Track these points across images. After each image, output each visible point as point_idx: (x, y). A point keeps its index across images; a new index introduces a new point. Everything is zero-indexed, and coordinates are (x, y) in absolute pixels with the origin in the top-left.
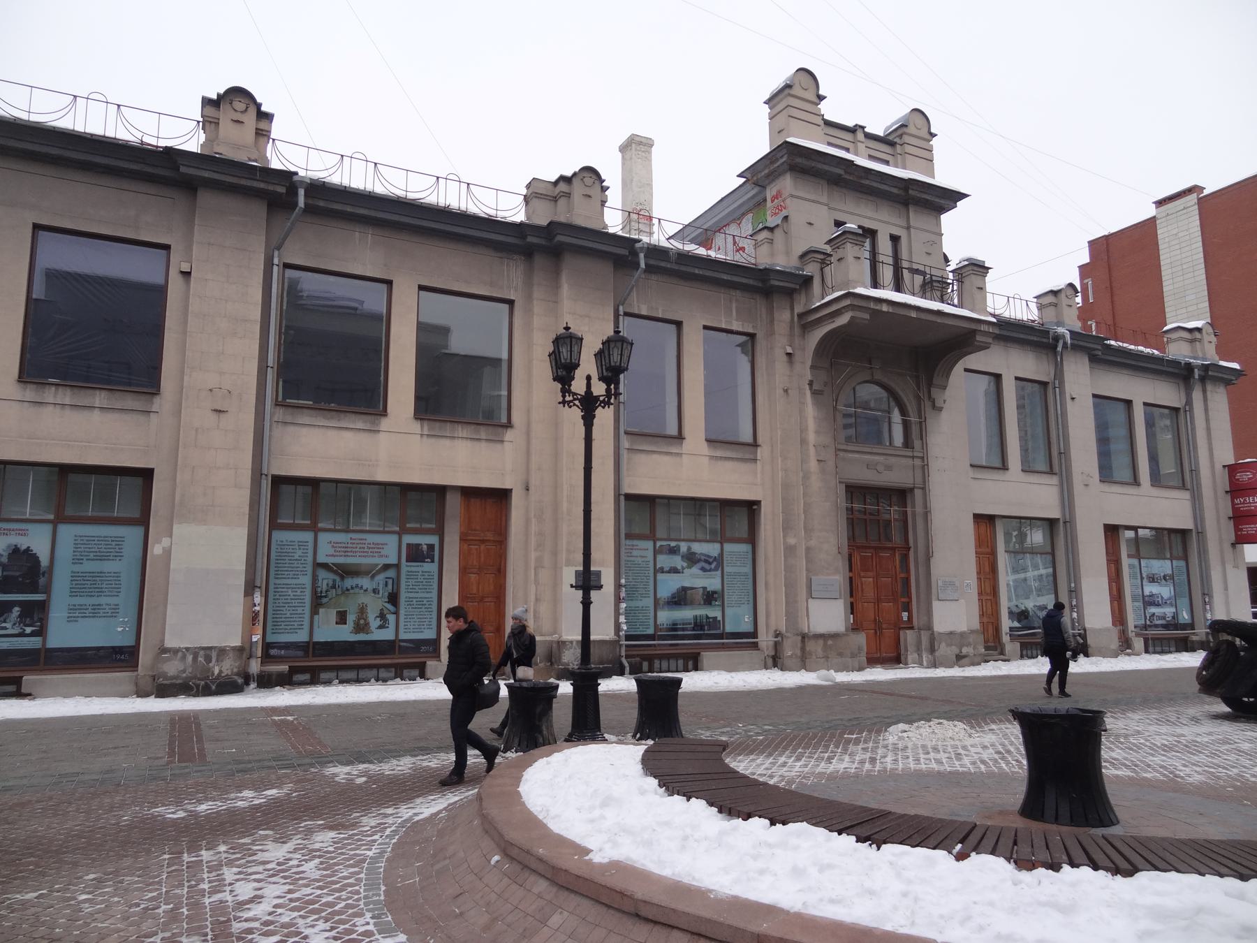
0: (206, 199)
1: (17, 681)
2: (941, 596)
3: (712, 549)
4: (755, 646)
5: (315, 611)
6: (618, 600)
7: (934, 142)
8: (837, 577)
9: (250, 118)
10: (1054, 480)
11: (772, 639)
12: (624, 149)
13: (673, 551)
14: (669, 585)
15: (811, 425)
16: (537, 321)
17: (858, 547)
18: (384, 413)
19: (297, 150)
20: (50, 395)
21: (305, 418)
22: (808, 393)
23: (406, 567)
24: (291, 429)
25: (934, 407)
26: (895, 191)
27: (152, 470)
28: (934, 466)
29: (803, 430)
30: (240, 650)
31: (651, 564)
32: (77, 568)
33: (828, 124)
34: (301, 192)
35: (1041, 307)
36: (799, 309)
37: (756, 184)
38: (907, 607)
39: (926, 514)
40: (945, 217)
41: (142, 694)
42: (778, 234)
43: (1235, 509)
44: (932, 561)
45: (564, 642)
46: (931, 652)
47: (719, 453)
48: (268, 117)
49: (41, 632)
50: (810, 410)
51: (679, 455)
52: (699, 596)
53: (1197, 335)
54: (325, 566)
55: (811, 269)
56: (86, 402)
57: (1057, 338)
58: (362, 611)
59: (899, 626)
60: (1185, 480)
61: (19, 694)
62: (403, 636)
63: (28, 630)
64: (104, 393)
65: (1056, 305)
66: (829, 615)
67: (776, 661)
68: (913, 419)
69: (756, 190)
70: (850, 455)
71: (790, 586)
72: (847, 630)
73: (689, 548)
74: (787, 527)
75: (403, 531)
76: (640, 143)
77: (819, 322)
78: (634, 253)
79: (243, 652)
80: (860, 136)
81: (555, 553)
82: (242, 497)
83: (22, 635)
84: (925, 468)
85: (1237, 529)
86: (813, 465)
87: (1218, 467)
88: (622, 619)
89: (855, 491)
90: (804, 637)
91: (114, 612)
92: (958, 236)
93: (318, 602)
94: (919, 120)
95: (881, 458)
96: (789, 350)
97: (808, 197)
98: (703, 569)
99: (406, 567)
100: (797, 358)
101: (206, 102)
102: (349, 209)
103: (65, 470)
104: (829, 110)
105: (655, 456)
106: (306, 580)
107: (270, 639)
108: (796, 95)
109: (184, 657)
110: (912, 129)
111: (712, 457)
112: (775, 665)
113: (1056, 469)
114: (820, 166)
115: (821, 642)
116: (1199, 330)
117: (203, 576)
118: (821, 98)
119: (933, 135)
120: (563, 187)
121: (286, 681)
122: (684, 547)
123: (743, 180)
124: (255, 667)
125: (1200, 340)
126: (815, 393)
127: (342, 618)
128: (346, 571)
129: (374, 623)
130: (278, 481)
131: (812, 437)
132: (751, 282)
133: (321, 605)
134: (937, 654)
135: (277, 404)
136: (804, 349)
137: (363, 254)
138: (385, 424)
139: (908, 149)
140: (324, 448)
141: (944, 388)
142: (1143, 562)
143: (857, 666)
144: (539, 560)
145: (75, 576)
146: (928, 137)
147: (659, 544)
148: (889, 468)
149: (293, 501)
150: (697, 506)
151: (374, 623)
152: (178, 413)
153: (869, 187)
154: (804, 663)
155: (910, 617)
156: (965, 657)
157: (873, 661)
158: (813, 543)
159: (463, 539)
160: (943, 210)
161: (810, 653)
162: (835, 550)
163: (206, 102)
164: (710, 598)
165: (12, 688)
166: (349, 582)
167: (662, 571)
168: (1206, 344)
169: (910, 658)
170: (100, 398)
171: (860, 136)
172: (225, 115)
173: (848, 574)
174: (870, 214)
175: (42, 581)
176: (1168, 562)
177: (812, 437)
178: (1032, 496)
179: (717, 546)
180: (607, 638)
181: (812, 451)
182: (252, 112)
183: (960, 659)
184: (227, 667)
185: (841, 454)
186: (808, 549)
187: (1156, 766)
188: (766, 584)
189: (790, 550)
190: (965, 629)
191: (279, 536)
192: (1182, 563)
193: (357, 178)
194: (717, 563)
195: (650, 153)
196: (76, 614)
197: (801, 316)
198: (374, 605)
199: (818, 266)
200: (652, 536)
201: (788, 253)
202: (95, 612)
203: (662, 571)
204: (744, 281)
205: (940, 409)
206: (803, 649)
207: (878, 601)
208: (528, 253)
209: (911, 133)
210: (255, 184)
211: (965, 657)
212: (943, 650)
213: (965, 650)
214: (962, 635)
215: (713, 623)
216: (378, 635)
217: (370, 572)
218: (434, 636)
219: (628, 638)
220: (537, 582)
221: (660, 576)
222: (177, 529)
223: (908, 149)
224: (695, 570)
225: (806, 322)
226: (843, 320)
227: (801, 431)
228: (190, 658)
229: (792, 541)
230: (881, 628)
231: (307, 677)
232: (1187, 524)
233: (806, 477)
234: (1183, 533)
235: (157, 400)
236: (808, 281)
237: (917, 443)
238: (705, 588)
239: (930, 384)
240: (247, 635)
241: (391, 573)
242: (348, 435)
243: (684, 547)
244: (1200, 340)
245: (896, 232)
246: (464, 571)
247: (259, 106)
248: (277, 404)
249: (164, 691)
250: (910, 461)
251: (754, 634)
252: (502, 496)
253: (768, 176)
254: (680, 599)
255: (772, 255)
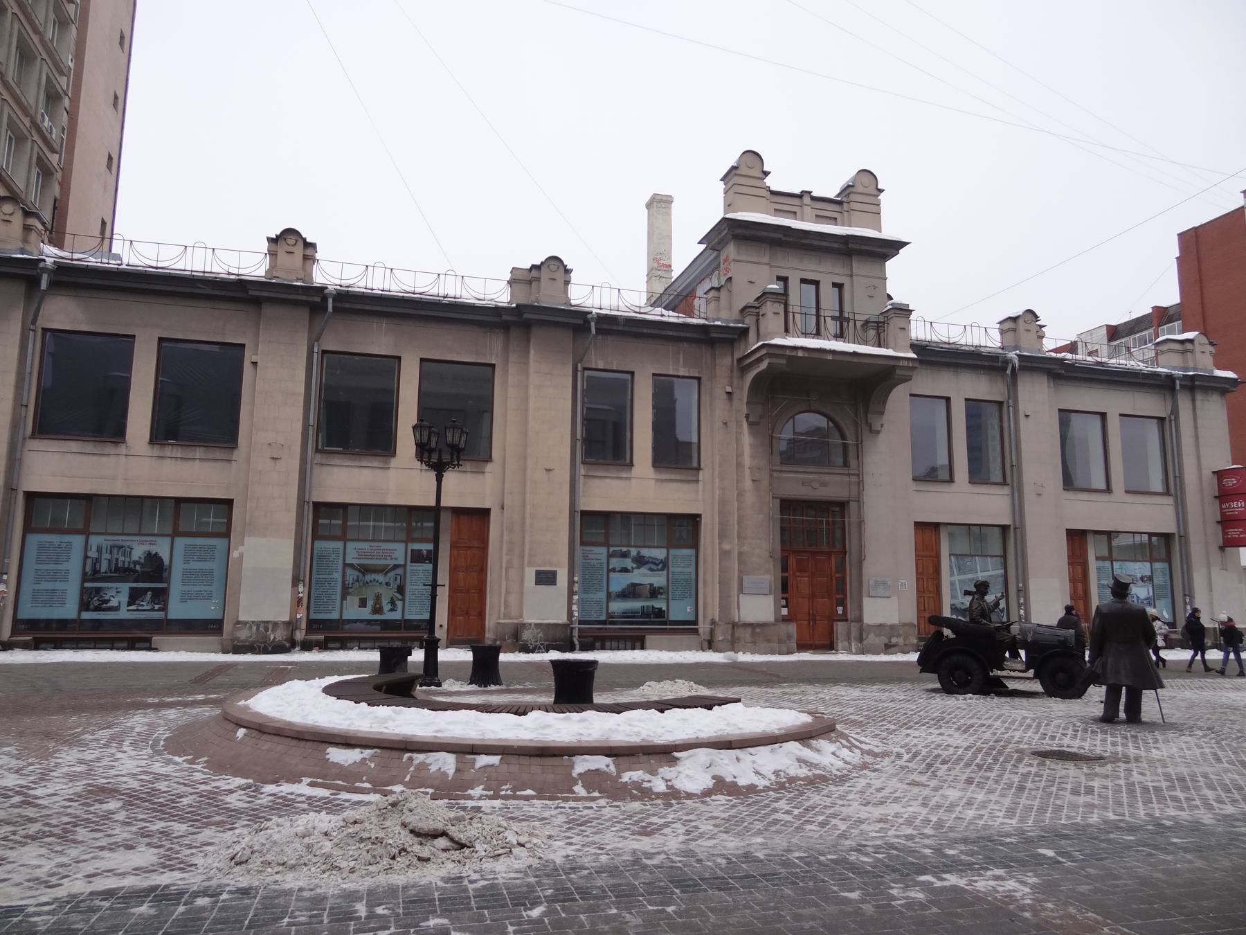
0: (268, 310)
1: (149, 640)
2: (872, 593)
3: (659, 554)
4: (696, 632)
5: (343, 598)
6: (571, 593)
7: (882, 197)
8: (768, 577)
9: (299, 251)
10: (1006, 490)
11: (708, 626)
12: (649, 205)
13: (625, 555)
14: (619, 582)
15: (747, 450)
16: (511, 380)
17: (794, 552)
18: (393, 454)
19: (329, 273)
20: (168, 451)
21: (337, 460)
22: (745, 425)
23: (410, 567)
24: (326, 469)
25: (871, 430)
26: (836, 246)
27: (232, 501)
28: (868, 481)
29: (739, 455)
30: (288, 624)
31: (605, 566)
32: (186, 566)
33: (774, 193)
34: (330, 301)
35: (1002, 332)
36: (737, 355)
37: (713, 249)
38: (842, 602)
39: (860, 523)
40: (889, 264)
41: (225, 652)
42: (723, 293)
43: (1222, 514)
44: (865, 565)
45: (524, 625)
46: (861, 640)
47: (664, 476)
48: (313, 246)
49: (164, 609)
50: (747, 439)
51: (629, 479)
52: (646, 591)
53: (1189, 346)
54: (351, 566)
55: (749, 321)
56: (190, 456)
57: (1007, 361)
58: (378, 598)
59: (832, 618)
60: (1173, 487)
61: (150, 649)
62: (407, 617)
63: (157, 607)
64: (202, 449)
65: (1015, 330)
66: (759, 607)
67: (710, 645)
68: (851, 441)
69: (715, 253)
70: (784, 475)
71: (724, 584)
72: (776, 620)
73: (639, 553)
74: (722, 536)
75: (409, 539)
76: (661, 201)
77: (751, 366)
78: (587, 322)
79: (292, 625)
80: (806, 200)
81: (522, 557)
82: (290, 518)
83: (153, 610)
84: (860, 483)
85: (1224, 534)
86: (748, 484)
87: (1207, 473)
88: (575, 608)
89: (788, 505)
90: (734, 625)
91: (209, 597)
92: (899, 279)
93: (345, 592)
94: (866, 179)
95: (815, 476)
96: (729, 389)
97: (749, 259)
98: (651, 570)
99: (410, 567)
100: (735, 396)
101: (270, 240)
102: (367, 308)
103: (179, 501)
104: (773, 183)
105: (608, 481)
106: (338, 576)
107: (313, 616)
108: (746, 173)
109: (251, 628)
110: (859, 188)
111: (657, 480)
112: (710, 648)
113: (1009, 480)
114: (864, 247)
115: (749, 630)
116: (1191, 341)
117: (264, 570)
118: (766, 174)
119: (881, 191)
120: (535, 273)
121: (324, 646)
122: (634, 552)
123: (704, 246)
124: (300, 636)
125: (1192, 351)
126: (750, 424)
127: (363, 603)
128: (365, 570)
129: (386, 607)
130: (318, 506)
131: (747, 461)
132: (695, 336)
133: (348, 593)
134: (865, 642)
135: (317, 451)
136: (742, 389)
137: (376, 340)
138: (394, 462)
139: (854, 206)
140: (349, 481)
141: (882, 413)
142: (1116, 565)
143: (785, 649)
144: (509, 562)
145: (186, 573)
146: (876, 192)
147: (612, 549)
148: (824, 484)
149: (325, 519)
150: (645, 518)
151: (386, 607)
152: (248, 460)
153: (811, 245)
154: (733, 645)
155: (845, 611)
156: (894, 646)
157: (802, 647)
158: (745, 548)
159: (453, 546)
160: (886, 257)
161: (739, 639)
162: (767, 554)
163: (270, 240)
164: (654, 592)
165: (147, 645)
166: (369, 577)
167: (614, 570)
168: (1198, 355)
169: (840, 645)
170: (199, 453)
171: (806, 200)
172: (281, 249)
173: (779, 574)
174: (812, 266)
175: (165, 575)
176: (1148, 565)
177: (747, 461)
178: (989, 506)
179: (664, 551)
180: (560, 622)
181: (747, 472)
182: (301, 244)
183: (888, 648)
184: (279, 635)
185: (775, 474)
186: (740, 554)
187: (445, 659)
188: (705, 582)
189: (725, 555)
190: (895, 621)
191: (318, 544)
192: (1166, 565)
193: (377, 283)
194: (664, 565)
195: (670, 208)
196: (186, 597)
197: (740, 360)
198: (387, 594)
199: (754, 318)
200: (607, 544)
201: (730, 308)
202: (199, 596)
203: (614, 570)
204: (688, 335)
205: (878, 432)
206: (733, 635)
207: (813, 597)
208: (505, 327)
209: (862, 192)
210: (300, 297)
211: (894, 646)
212: (871, 639)
213: (894, 640)
214: (892, 627)
215: (660, 613)
216: (388, 616)
217: (384, 570)
218: (427, 616)
219: (581, 622)
220: (507, 579)
221: (612, 575)
222: (246, 539)
223: (854, 206)
224: (644, 570)
225: (742, 366)
226: (764, 366)
227: (737, 456)
228: (254, 628)
229: (726, 547)
230: (815, 620)
231: (338, 645)
232: (1170, 528)
233: (741, 494)
234: (1167, 537)
235: (236, 452)
236: (745, 332)
237: (853, 462)
238: (651, 585)
239: (866, 412)
240: (293, 612)
241: (400, 571)
242: (366, 471)
243: (634, 552)
244: (1192, 351)
245: (838, 280)
246: (453, 570)
247: (304, 240)
248: (317, 451)
249: (237, 650)
250: (846, 479)
251: (695, 622)
252: (484, 513)
253: (719, 243)
254: (631, 592)
255: (718, 310)
